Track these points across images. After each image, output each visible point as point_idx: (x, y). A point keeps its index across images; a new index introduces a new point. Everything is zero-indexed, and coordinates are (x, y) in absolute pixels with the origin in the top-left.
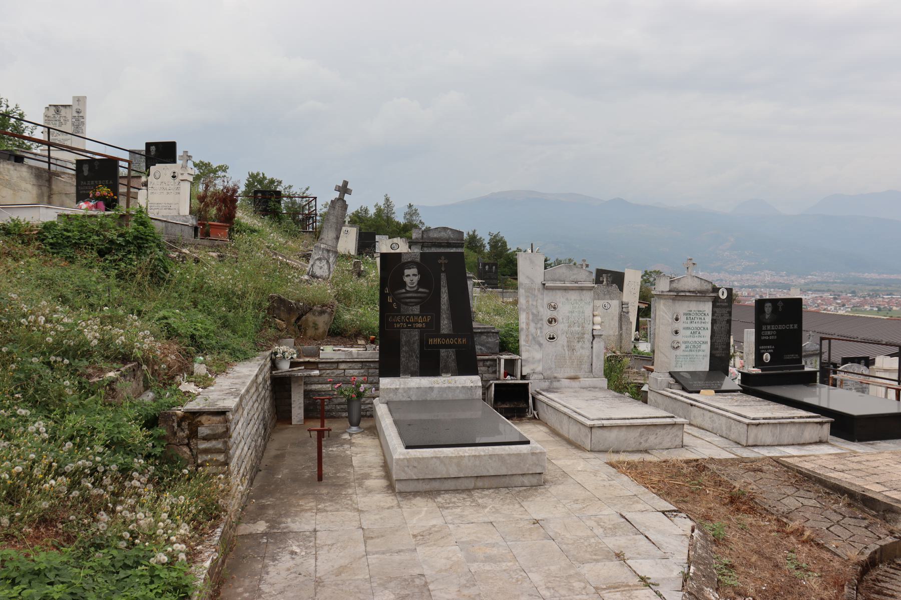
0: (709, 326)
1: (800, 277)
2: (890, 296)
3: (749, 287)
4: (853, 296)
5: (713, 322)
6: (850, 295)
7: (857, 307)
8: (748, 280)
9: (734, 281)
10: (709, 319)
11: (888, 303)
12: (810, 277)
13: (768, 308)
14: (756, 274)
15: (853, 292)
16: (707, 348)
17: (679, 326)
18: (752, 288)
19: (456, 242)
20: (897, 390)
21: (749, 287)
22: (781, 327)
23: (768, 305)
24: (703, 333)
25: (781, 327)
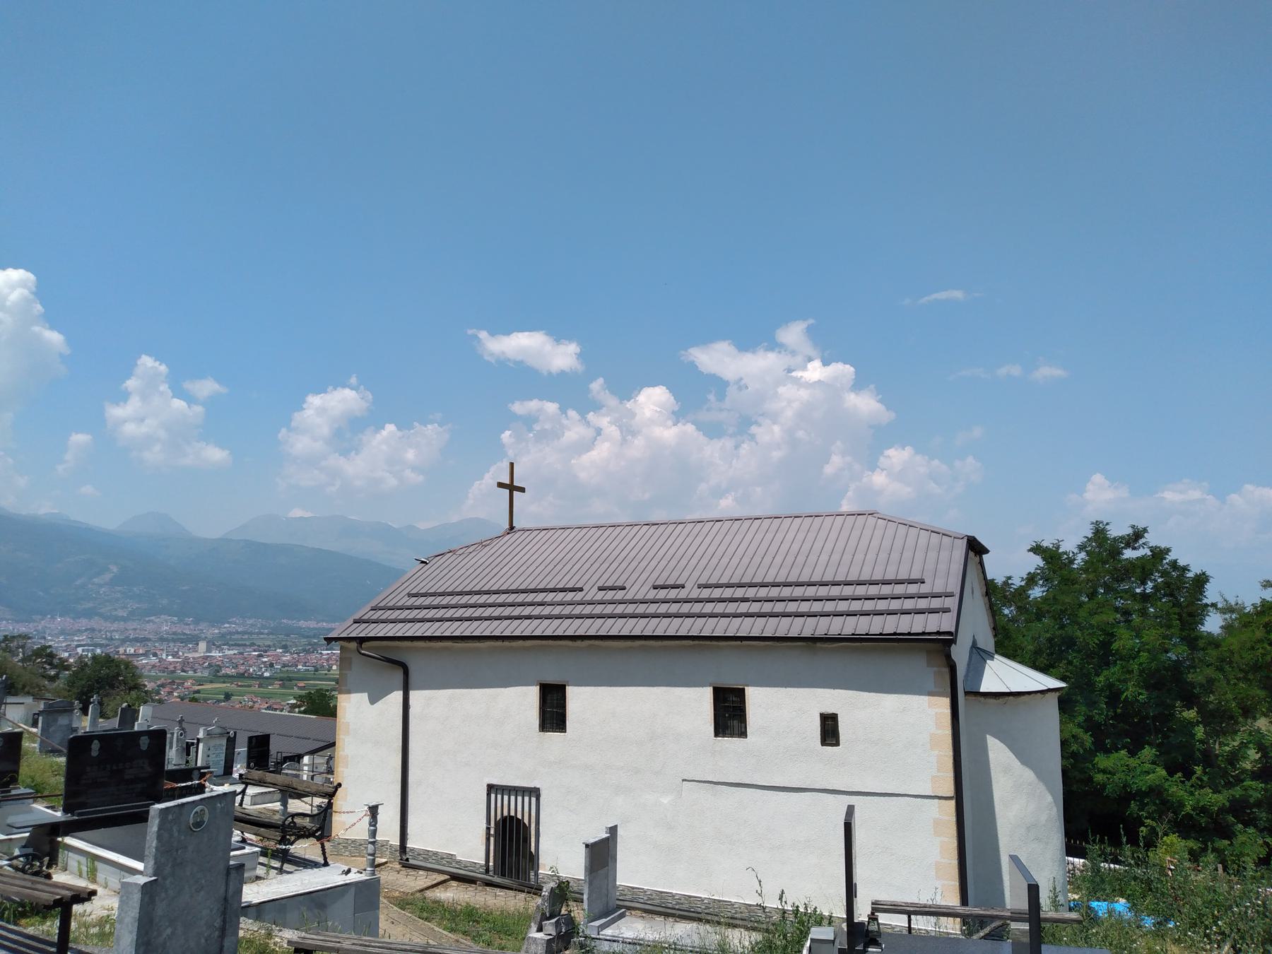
0: (224, 751)
1: (213, 626)
2: (329, 652)
3: (136, 640)
4: (284, 652)
5: (226, 749)
6: (281, 650)
7: (288, 666)
8: (135, 629)
9: (113, 631)
10: (224, 748)
11: (328, 660)
12: (227, 625)
13: (254, 741)
14: (148, 622)
15: (285, 647)
16: (223, 763)
17: (210, 753)
18: (141, 642)
19: (888, 907)
20: (833, 942)
21: (136, 640)
22: (260, 749)
23: (254, 738)
24: (221, 755)
25: (260, 749)
